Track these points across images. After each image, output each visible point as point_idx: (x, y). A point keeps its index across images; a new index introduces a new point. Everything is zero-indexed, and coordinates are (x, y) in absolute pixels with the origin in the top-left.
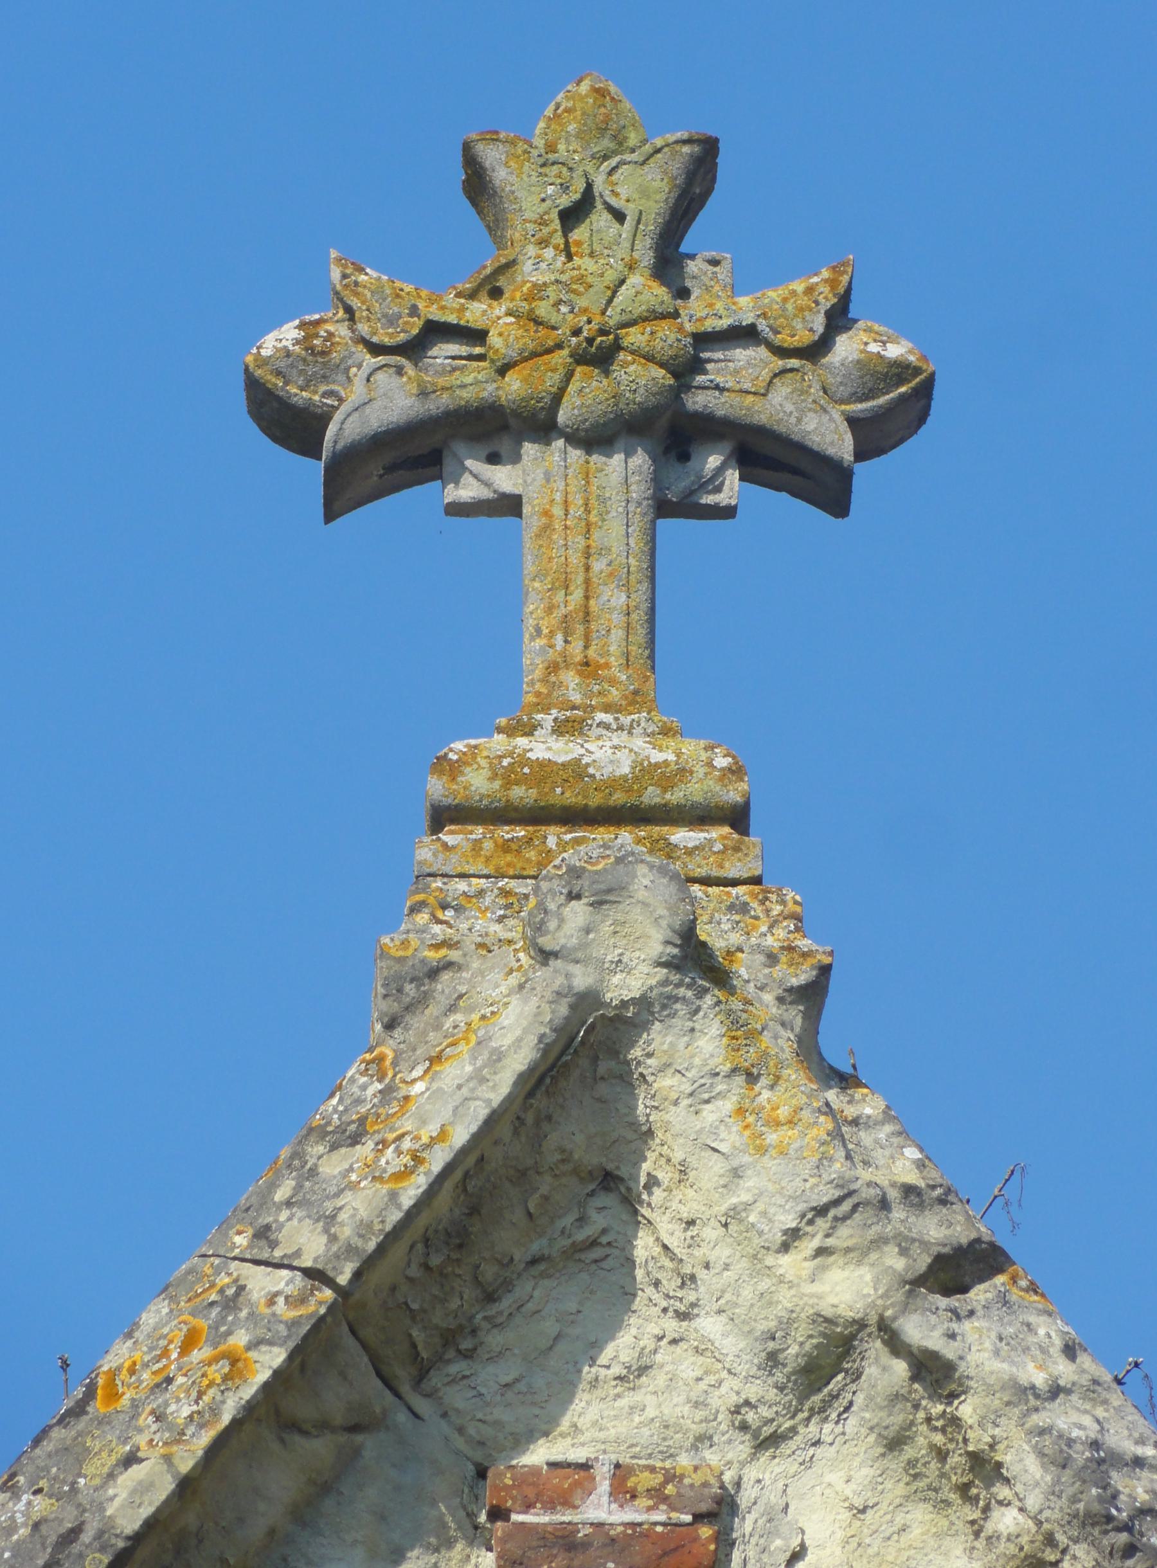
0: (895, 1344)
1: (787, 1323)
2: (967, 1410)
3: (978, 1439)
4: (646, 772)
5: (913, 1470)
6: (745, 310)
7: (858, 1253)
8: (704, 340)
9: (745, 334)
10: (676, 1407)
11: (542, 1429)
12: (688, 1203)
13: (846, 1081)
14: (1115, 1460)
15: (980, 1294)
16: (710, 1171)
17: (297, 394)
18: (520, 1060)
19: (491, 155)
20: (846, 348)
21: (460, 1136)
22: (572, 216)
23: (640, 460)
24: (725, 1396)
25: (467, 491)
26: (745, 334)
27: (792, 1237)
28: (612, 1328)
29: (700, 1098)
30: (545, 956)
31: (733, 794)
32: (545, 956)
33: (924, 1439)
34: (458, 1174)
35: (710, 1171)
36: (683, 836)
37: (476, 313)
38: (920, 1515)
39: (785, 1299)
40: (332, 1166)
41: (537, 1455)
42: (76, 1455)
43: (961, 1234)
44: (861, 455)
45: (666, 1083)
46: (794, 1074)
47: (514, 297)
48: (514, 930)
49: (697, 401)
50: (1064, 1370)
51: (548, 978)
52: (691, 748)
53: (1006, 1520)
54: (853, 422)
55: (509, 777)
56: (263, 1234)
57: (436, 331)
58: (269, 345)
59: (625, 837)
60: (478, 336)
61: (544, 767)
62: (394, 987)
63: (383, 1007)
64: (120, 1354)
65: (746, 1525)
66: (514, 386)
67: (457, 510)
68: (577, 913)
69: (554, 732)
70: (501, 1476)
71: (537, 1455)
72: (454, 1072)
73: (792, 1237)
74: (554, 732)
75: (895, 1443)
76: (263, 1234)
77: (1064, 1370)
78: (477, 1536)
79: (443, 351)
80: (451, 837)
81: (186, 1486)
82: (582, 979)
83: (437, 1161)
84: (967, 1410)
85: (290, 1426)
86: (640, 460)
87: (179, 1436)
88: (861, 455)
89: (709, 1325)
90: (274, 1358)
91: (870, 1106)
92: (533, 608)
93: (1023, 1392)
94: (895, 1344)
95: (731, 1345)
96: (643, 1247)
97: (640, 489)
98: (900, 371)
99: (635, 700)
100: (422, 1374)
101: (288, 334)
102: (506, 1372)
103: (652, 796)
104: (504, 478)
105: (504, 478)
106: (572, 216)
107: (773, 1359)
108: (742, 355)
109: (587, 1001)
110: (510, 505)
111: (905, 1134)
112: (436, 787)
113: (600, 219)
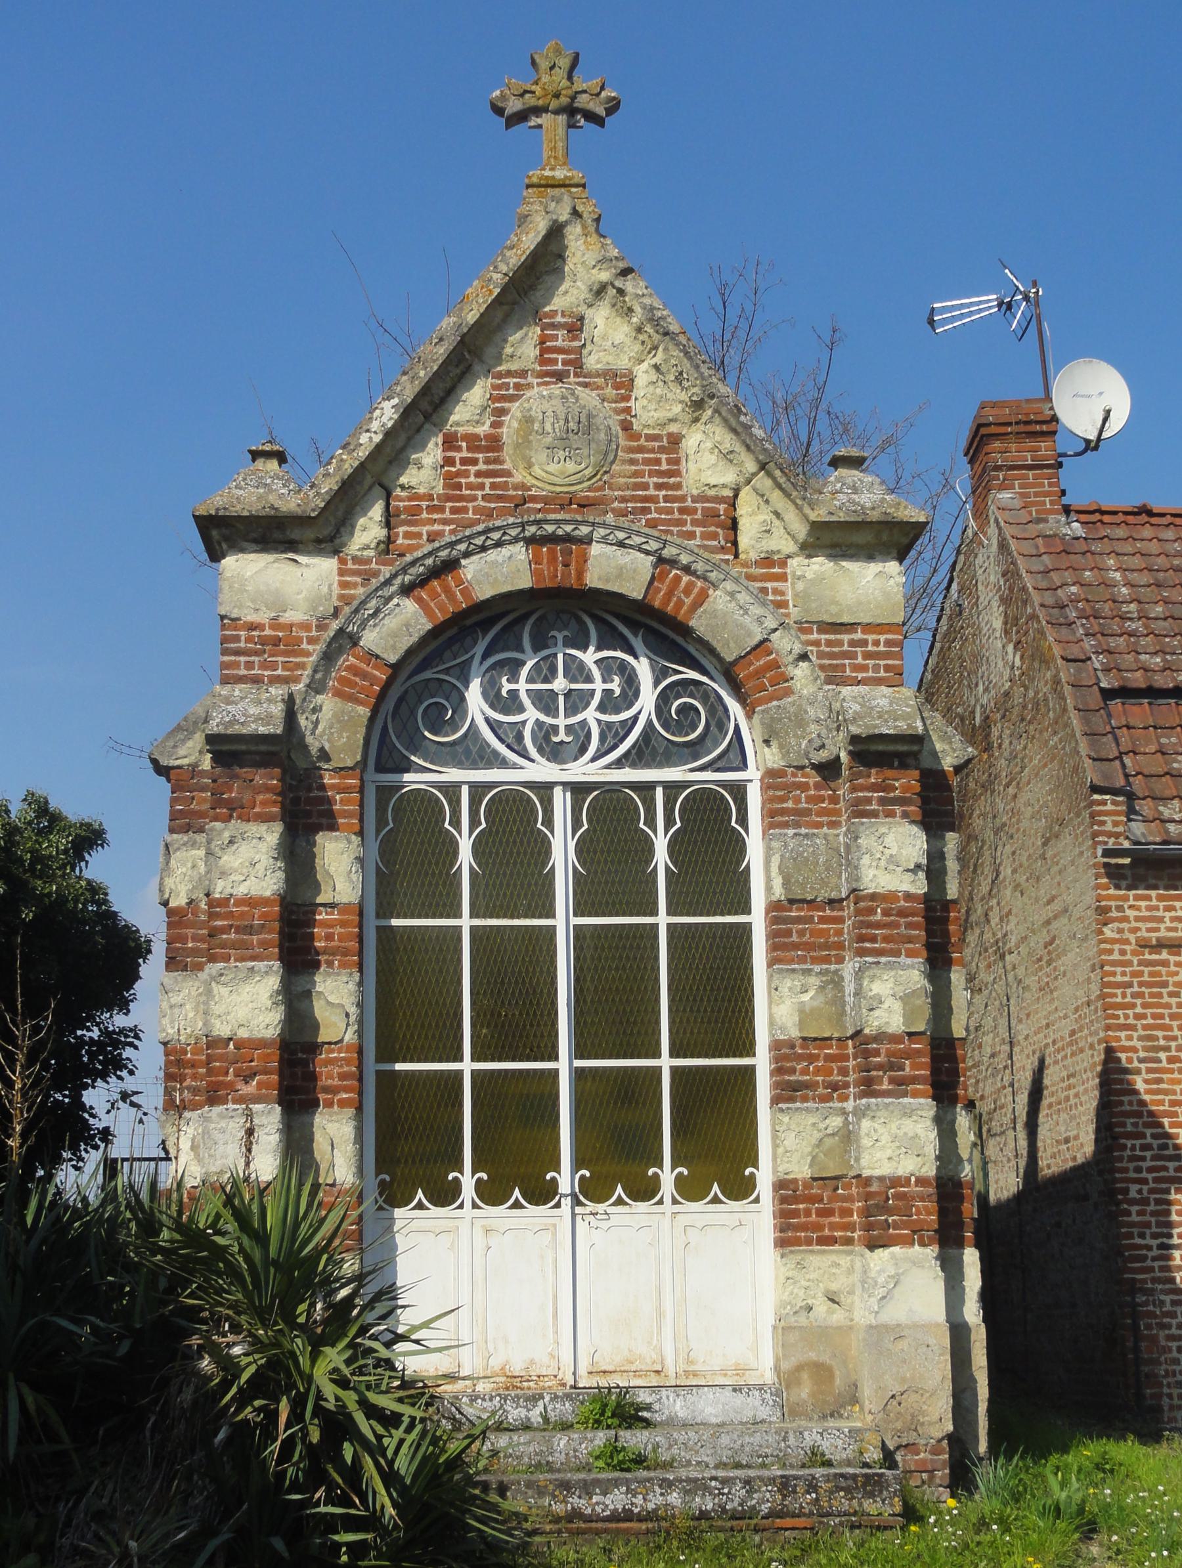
0: (614, 286)
1: (593, 283)
2: (627, 299)
3: (629, 304)
4: (566, 177)
5: (617, 311)
6: (585, 86)
7: (607, 269)
8: (577, 93)
9: (585, 92)
10: (573, 299)
11: (549, 303)
12: (575, 260)
13: (604, 237)
14: (655, 308)
15: (629, 277)
16: (579, 254)
17: (500, 104)
18: (543, 233)
19: (536, 57)
20: (603, 94)
21: (532, 248)
22: (552, 68)
23: (565, 117)
24: (582, 297)
25: (532, 123)
26: (585, 92)
27: (594, 266)
28: (561, 285)
29: (577, 240)
30: (547, 213)
31: (583, 182)
32: (547, 213)
33: (619, 304)
34: (607, 788)
35: (579, 254)
36: (573, 190)
37: (533, 88)
38: (618, 319)
39: (593, 278)
40: (508, 253)
41: (547, 309)
42: (461, 310)
43: (626, 266)
44: (607, 115)
45: (571, 237)
46: (594, 235)
47: (541, 84)
48: (542, 208)
49: (576, 105)
50: (645, 291)
51: (549, 216)
52: (575, 173)
53: (635, 320)
54: (606, 109)
55: (541, 179)
56: (496, 267)
57: (526, 92)
58: (494, 95)
59: (563, 190)
60: (533, 92)
61: (547, 177)
62: (519, 219)
63: (517, 223)
64: (470, 290)
65: (586, 321)
66: (541, 102)
67: (530, 127)
68: (553, 204)
69: (793, 693)
70: (541, 313)
71: (547, 309)
72: (531, 235)
73: (594, 266)
74: (793, 693)
75: (614, 306)
76: (496, 267)
77: (645, 291)
78: (536, 324)
79: (527, 96)
80: (530, 190)
81: (482, 315)
82: (554, 217)
83: (528, 252)
84: (627, 299)
85: (501, 304)
86: (565, 117)
87: (480, 305)
88: (607, 115)
89: (579, 284)
90: (498, 290)
91: (609, 242)
92: (545, 146)
93: (637, 295)
94: (614, 286)
95: (583, 287)
96: (566, 269)
97: (565, 122)
98: (614, 98)
99: (564, 164)
100: (526, 293)
101: (497, 93)
102: (542, 292)
103: (567, 182)
104: (539, 121)
105: (539, 121)
106: (552, 68)
107: (591, 290)
108: (584, 96)
109: (555, 221)
110: (540, 126)
111: (616, 247)
112: (527, 181)
113: (557, 69)
